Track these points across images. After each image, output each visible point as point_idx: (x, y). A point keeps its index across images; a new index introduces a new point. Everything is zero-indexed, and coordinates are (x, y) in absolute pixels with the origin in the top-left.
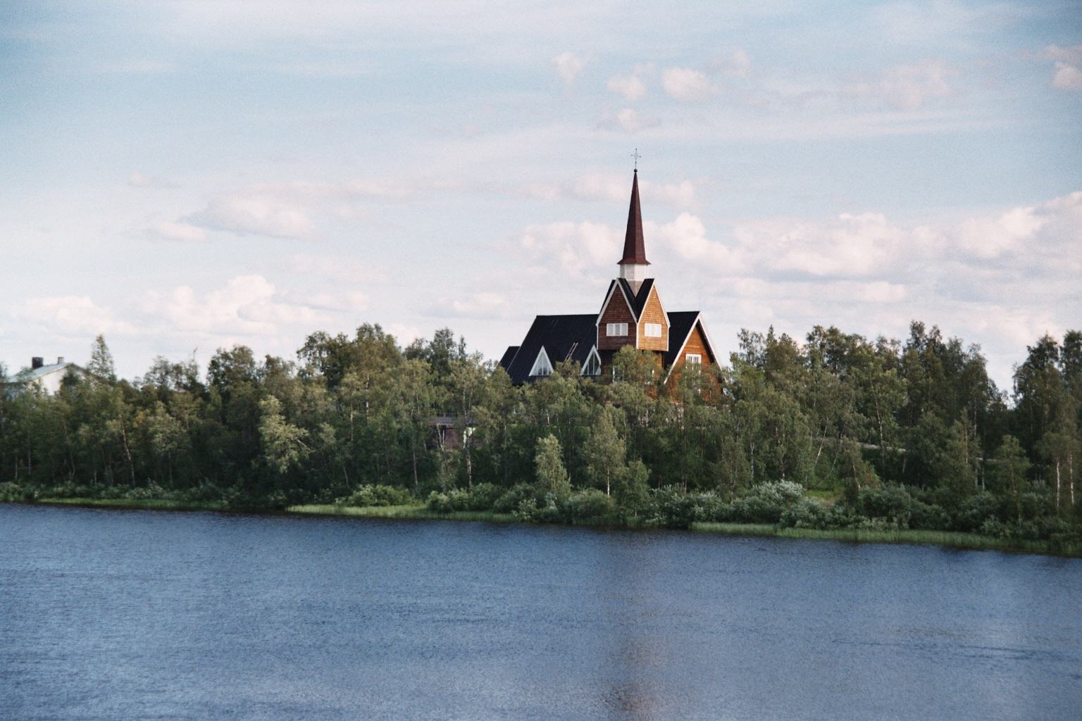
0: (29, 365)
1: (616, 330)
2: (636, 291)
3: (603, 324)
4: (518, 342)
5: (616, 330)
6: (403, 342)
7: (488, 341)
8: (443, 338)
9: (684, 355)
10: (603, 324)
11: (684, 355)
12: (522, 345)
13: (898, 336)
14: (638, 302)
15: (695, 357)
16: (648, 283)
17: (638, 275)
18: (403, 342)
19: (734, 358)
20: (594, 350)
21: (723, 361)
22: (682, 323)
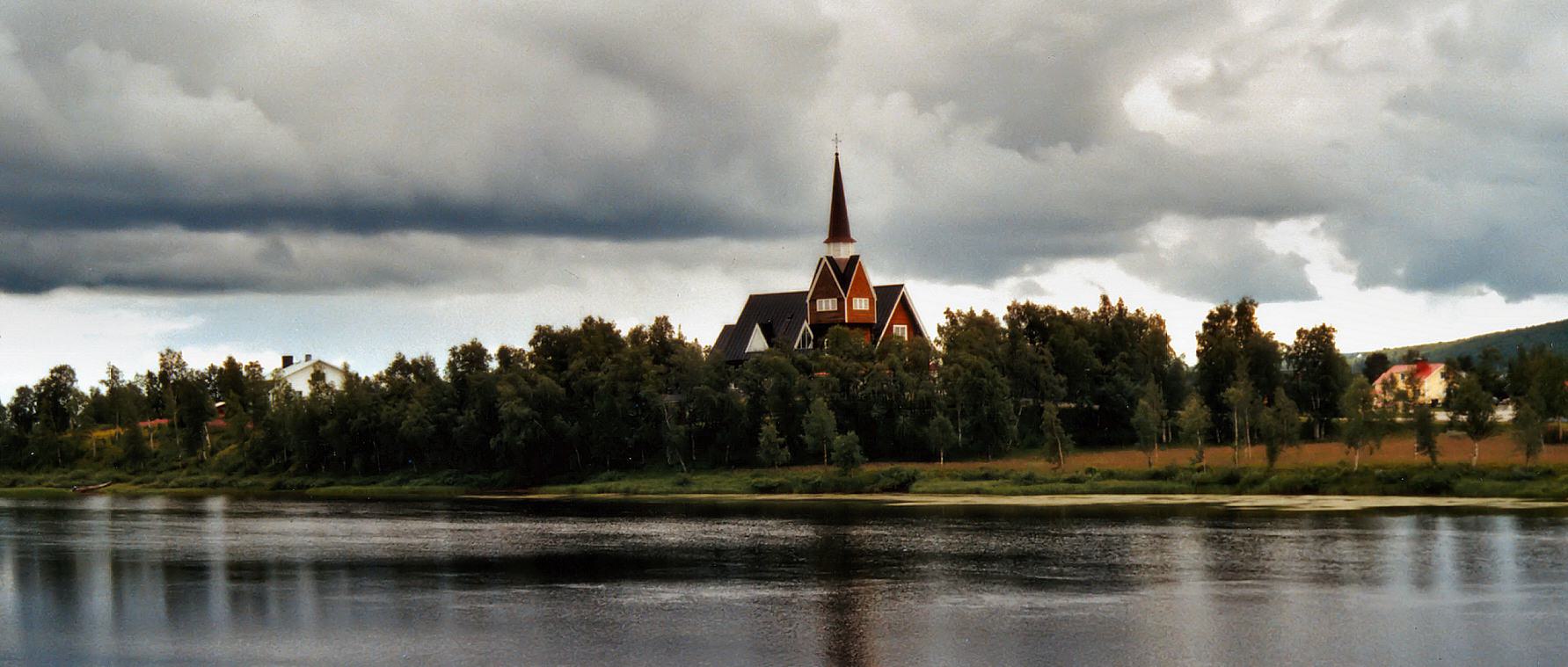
0: (280, 365)
1: (827, 305)
2: (842, 269)
3: (813, 301)
4: (734, 321)
5: (827, 305)
6: (624, 329)
7: (372, 378)
8: (662, 325)
9: (890, 328)
10: (813, 301)
11: (890, 328)
12: (717, 343)
13: (576, 324)
14: (845, 279)
15: (901, 330)
16: (854, 259)
17: (844, 252)
18: (624, 329)
19: (940, 329)
20: (806, 325)
21: (931, 334)
22: (504, 353)
